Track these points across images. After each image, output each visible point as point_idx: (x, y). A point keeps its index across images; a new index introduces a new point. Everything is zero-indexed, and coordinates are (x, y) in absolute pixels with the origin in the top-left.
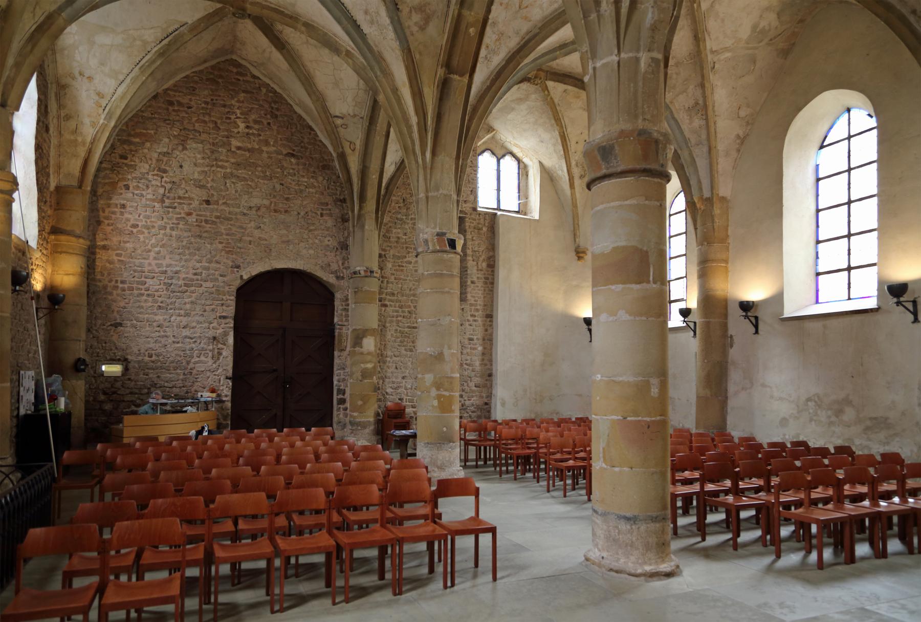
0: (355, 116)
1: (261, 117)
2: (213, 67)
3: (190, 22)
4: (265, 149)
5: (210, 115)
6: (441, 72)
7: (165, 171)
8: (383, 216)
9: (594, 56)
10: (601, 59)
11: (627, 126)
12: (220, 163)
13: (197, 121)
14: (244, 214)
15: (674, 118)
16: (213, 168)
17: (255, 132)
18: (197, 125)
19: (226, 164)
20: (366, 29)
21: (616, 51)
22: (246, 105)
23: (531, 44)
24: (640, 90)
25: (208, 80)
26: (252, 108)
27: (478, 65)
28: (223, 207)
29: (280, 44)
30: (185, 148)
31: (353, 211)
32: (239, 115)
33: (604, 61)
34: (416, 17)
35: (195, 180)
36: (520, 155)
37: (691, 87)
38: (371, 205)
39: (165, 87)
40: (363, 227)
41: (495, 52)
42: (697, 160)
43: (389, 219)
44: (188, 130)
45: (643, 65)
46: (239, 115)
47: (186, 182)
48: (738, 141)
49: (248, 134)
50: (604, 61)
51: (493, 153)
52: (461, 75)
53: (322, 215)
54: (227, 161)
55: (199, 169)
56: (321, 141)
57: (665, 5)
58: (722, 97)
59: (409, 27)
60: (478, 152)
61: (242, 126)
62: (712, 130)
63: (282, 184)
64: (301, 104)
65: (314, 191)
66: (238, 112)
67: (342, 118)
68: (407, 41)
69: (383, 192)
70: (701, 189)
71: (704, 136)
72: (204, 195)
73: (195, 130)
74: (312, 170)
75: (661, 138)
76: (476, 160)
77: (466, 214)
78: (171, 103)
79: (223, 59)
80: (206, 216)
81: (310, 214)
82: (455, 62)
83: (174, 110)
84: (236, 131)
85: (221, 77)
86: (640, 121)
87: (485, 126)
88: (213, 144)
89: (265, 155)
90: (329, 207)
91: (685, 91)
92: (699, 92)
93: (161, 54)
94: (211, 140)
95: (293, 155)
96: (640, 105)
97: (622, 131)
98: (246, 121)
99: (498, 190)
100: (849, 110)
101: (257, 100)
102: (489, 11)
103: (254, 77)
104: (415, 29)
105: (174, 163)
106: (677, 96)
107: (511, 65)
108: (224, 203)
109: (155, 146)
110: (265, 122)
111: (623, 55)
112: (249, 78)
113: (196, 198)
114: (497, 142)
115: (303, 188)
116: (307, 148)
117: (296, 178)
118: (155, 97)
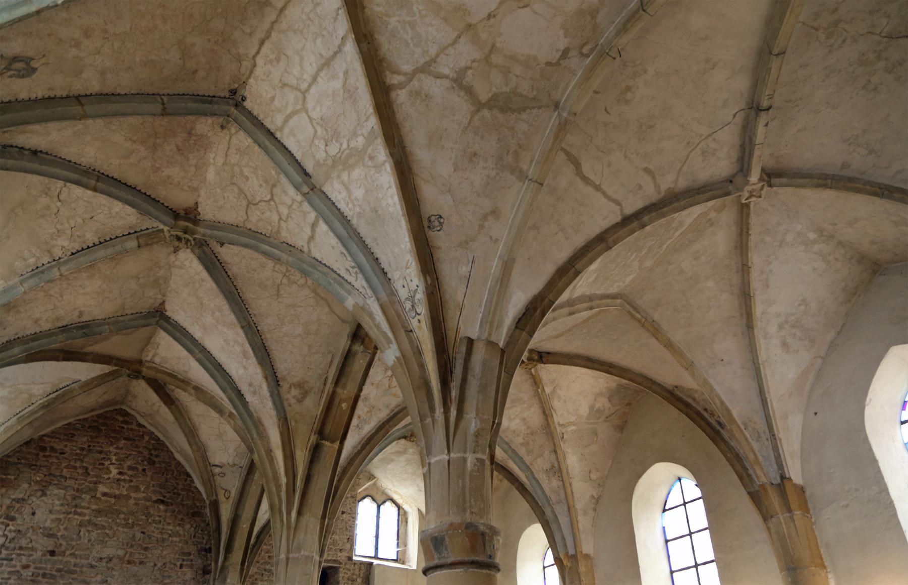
0: (234, 465)
1: (138, 463)
2: (99, 416)
3: (83, 379)
4: (133, 495)
5: (82, 461)
6: (314, 438)
7: (13, 519)
8: (249, 567)
9: (429, 453)
10: (435, 456)
11: (457, 519)
12: (79, 510)
13: (66, 467)
14: (92, 566)
15: (535, 478)
16: (70, 516)
17: (127, 478)
18: (65, 470)
19: (85, 511)
20: (249, 397)
21: (446, 452)
22: (124, 451)
23: (399, 416)
24: (468, 486)
25: (89, 427)
26: (130, 455)
27: (350, 432)
28: (68, 559)
29: (169, 400)
30: (44, 494)
31: (216, 562)
32: (114, 461)
33: (438, 458)
34: (295, 392)
35: (45, 528)
36: (400, 501)
37: (547, 452)
38: (237, 556)
39: (42, 433)
40: (225, 580)
41: (365, 422)
42: (559, 517)
43: (256, 570)
44: (54, 476)
45: (469, 465)
46: (114, 461)
47: (34, 530)
48: (593, 501)
49: (118, 480)
50: (438, 458)
51: (374, 500)
52: (333, 442)
53: (181, 566)
54: (88, 508)
55: (53, 517)
56: (196, 488)
57: (486, 417)
58: (573, 462)
59: (287, 400)
60: (359, 497)
61: (114, 471)
62: (569, 491)
63: (143, 533)
64: (182, 452)
65: (178, 539)
66: (114, 458)
67: (221, 467)
68: (285, 411)
69: (252, 541)
70: (565, 545)
71: (563, 496)
72: (49, 544)
73: (61, 476)
74: (180, 517)
75: (487, 531)
76: (356, 507)
77: (340, 563)
78: (43, 449)
79: (111, 408)
80: (45, 569)
81: (168, 565)
82: (328, 429)
83: (44, 456)
84: (106, 476)
85: (105, 424)
86: (468, 514)
87: (366, 474)
88: (78, 490)
89: (132, 502)
90: (192, 557)
91: (542, 455)
92: (553, 457)
93: (44, 406)
94: (76, 486)
95: (162, 502)
96: (467, 499)
97: (451, 524)
98: (120, 466)
99: (377, 537)
100: (680, 479)
101: (137, 447)
102: (360, 390)
103: (140, 425)
104: (293, 401)
105: (27, 510)
106: (536, 458)
107: (381, 433)
108: (71, 554)
109: (11, 492)
110: (140, 468)
111: (452, 455)
112: (134, 426)
113: (40, 548)
114: (377, 489)
115: (165, 536)
116: (179, 495)
117: (160, 526)
118: (28, 443)
